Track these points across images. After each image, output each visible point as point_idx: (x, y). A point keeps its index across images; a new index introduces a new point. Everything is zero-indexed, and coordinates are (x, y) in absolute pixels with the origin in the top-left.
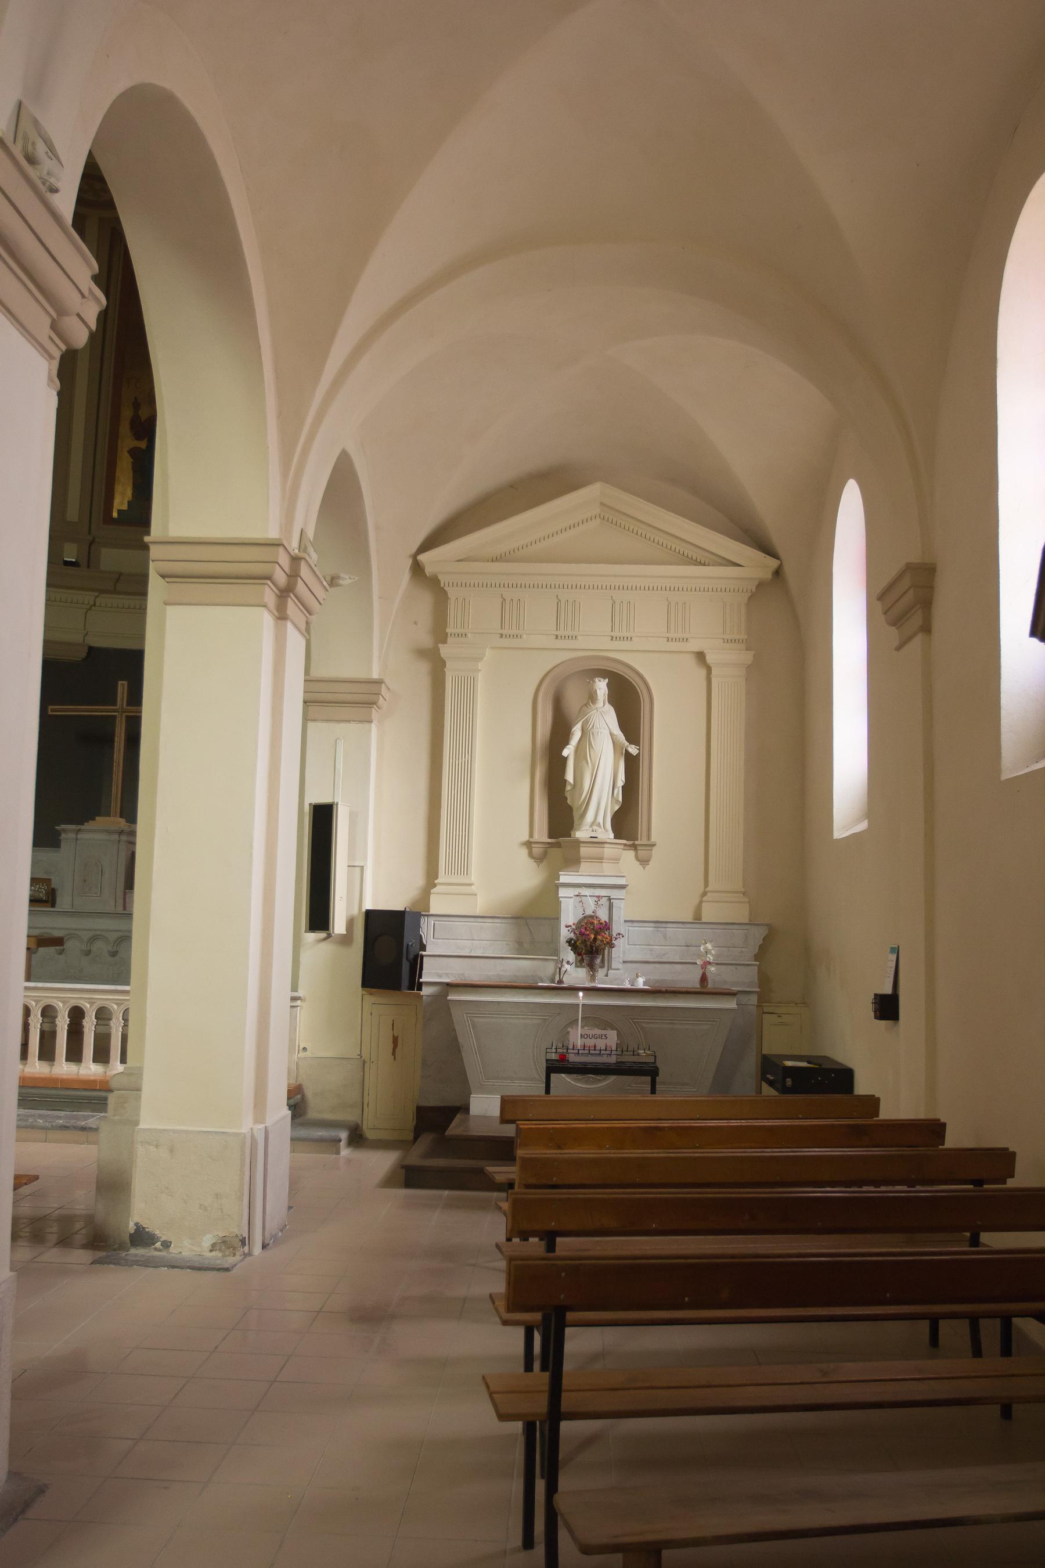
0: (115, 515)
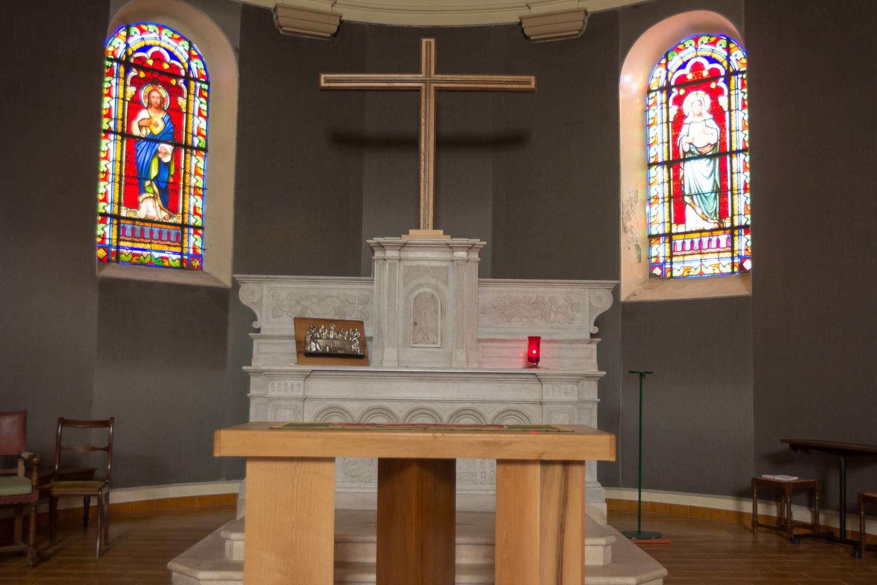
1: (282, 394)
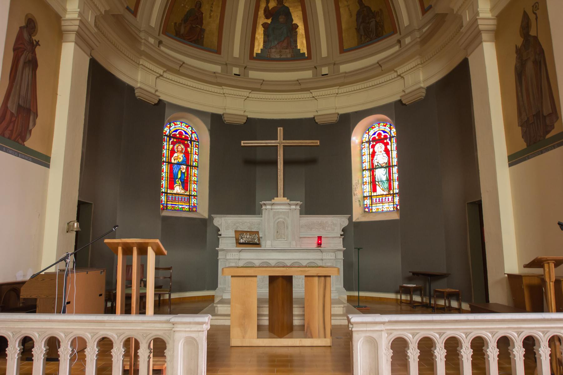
0: (255, 55)
1: (231, 258)
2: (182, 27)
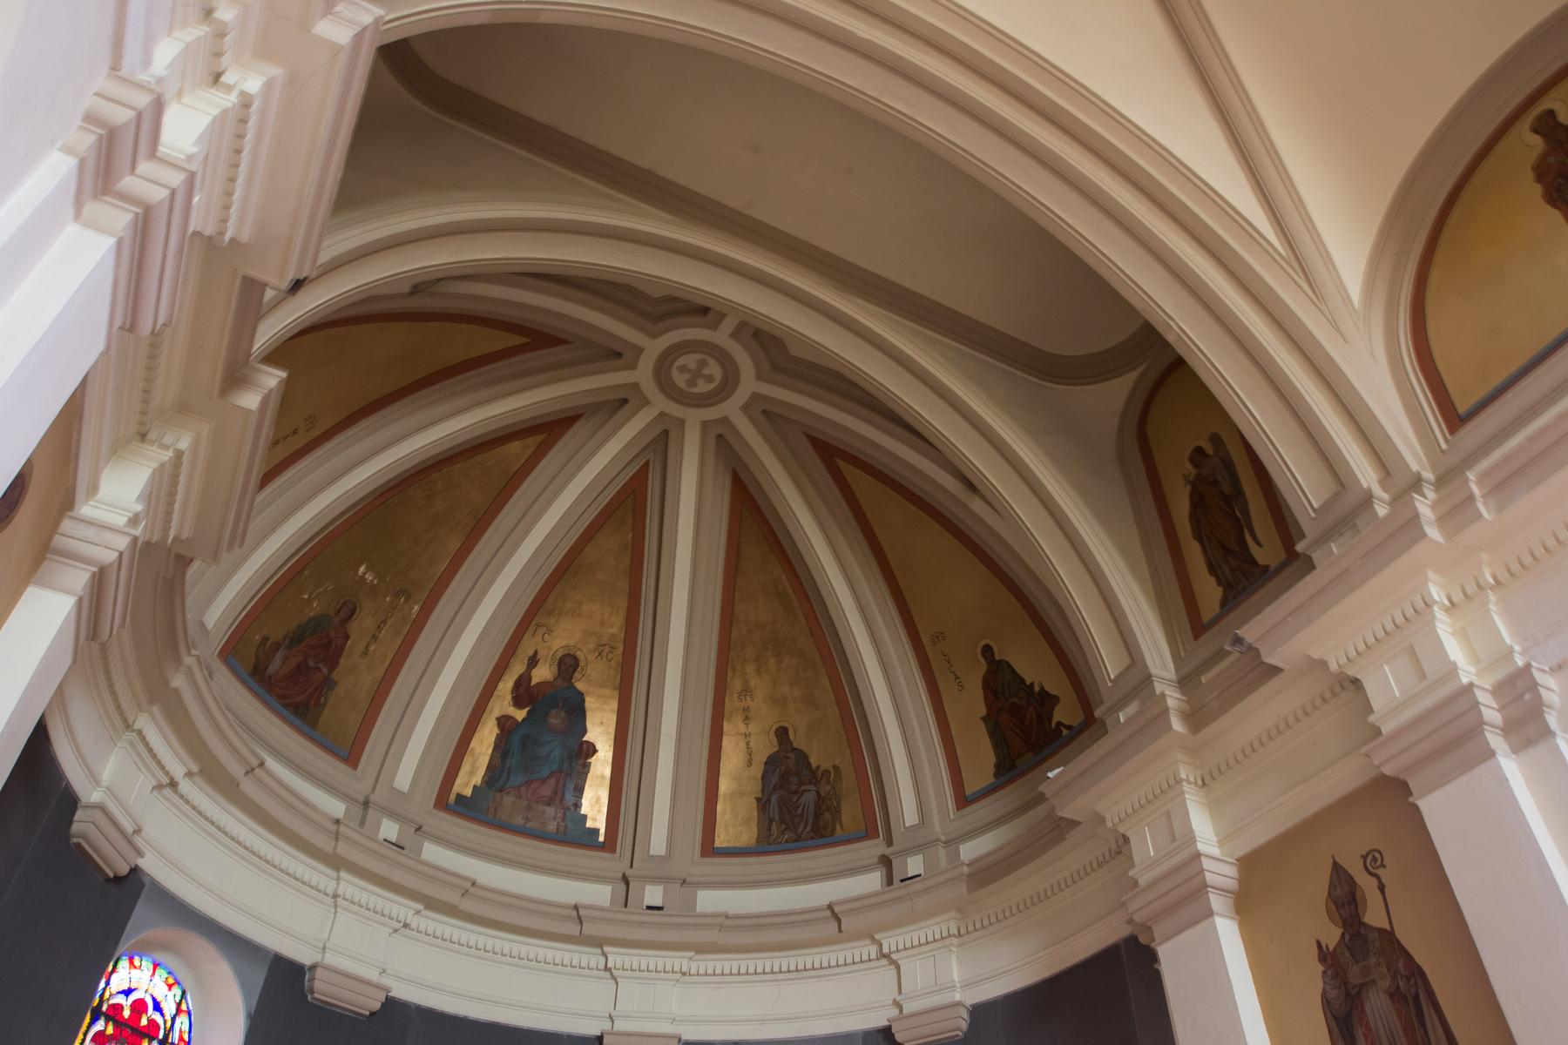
0: (452, 797)
2: (279, 656)
